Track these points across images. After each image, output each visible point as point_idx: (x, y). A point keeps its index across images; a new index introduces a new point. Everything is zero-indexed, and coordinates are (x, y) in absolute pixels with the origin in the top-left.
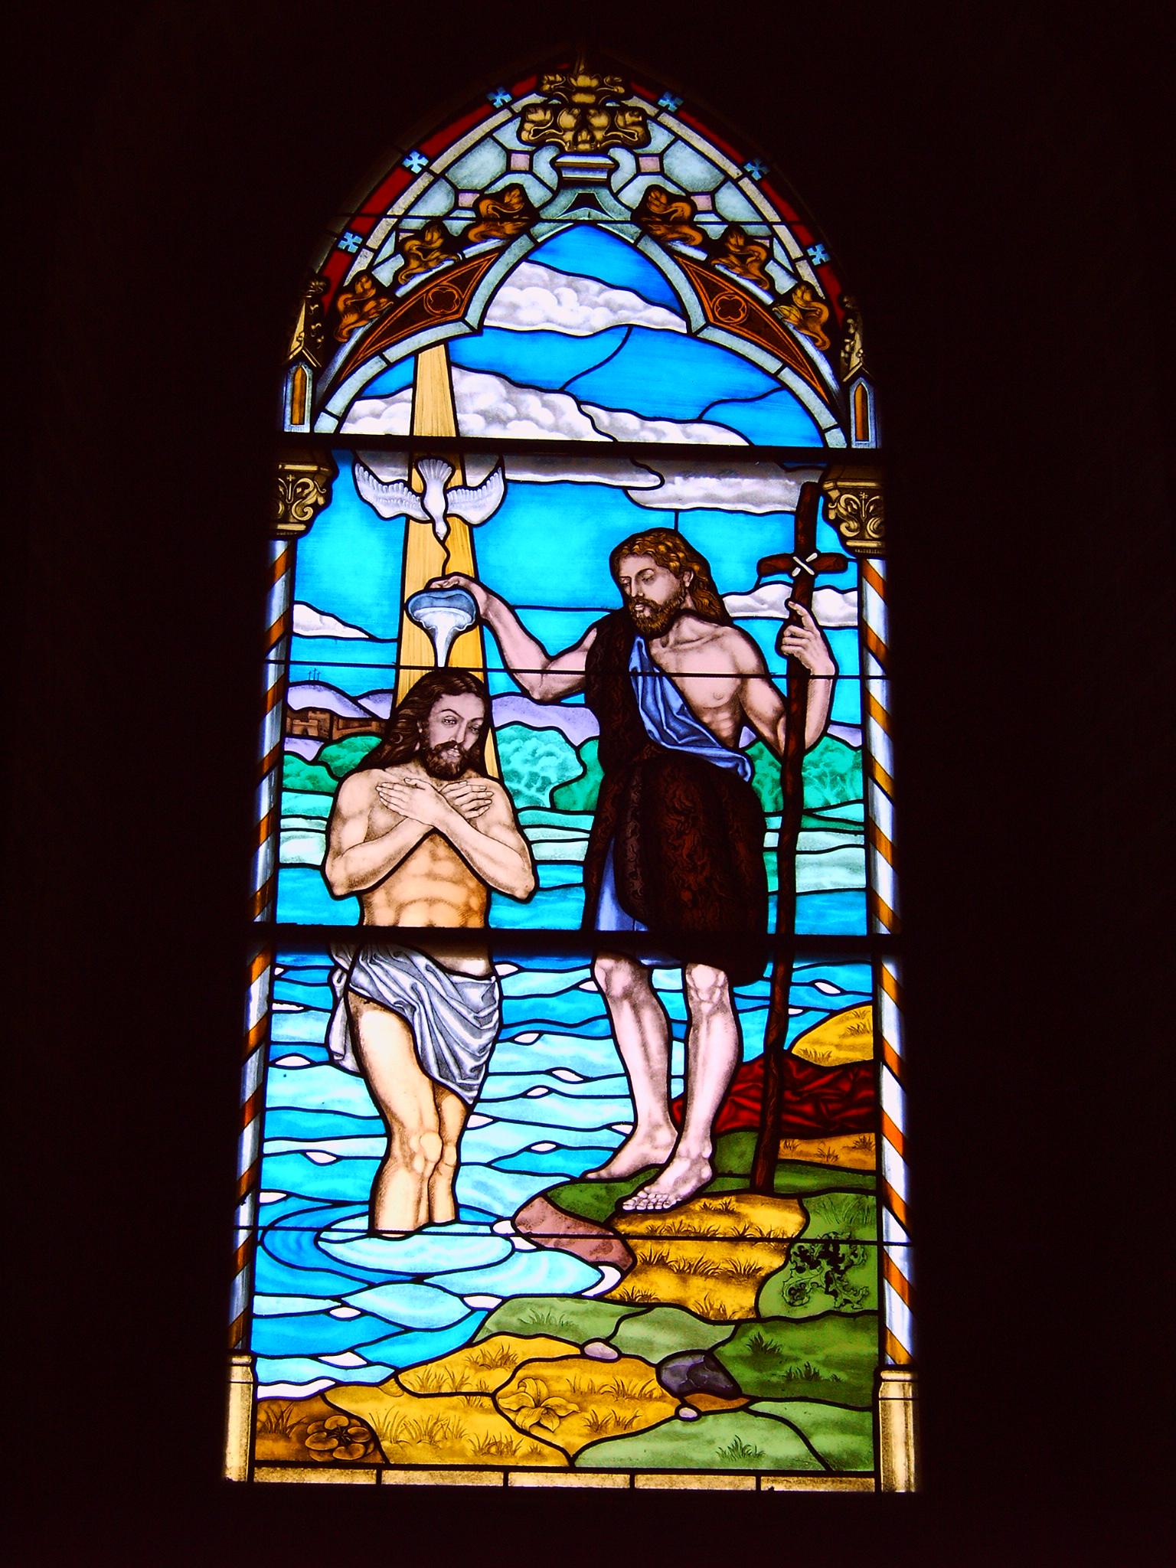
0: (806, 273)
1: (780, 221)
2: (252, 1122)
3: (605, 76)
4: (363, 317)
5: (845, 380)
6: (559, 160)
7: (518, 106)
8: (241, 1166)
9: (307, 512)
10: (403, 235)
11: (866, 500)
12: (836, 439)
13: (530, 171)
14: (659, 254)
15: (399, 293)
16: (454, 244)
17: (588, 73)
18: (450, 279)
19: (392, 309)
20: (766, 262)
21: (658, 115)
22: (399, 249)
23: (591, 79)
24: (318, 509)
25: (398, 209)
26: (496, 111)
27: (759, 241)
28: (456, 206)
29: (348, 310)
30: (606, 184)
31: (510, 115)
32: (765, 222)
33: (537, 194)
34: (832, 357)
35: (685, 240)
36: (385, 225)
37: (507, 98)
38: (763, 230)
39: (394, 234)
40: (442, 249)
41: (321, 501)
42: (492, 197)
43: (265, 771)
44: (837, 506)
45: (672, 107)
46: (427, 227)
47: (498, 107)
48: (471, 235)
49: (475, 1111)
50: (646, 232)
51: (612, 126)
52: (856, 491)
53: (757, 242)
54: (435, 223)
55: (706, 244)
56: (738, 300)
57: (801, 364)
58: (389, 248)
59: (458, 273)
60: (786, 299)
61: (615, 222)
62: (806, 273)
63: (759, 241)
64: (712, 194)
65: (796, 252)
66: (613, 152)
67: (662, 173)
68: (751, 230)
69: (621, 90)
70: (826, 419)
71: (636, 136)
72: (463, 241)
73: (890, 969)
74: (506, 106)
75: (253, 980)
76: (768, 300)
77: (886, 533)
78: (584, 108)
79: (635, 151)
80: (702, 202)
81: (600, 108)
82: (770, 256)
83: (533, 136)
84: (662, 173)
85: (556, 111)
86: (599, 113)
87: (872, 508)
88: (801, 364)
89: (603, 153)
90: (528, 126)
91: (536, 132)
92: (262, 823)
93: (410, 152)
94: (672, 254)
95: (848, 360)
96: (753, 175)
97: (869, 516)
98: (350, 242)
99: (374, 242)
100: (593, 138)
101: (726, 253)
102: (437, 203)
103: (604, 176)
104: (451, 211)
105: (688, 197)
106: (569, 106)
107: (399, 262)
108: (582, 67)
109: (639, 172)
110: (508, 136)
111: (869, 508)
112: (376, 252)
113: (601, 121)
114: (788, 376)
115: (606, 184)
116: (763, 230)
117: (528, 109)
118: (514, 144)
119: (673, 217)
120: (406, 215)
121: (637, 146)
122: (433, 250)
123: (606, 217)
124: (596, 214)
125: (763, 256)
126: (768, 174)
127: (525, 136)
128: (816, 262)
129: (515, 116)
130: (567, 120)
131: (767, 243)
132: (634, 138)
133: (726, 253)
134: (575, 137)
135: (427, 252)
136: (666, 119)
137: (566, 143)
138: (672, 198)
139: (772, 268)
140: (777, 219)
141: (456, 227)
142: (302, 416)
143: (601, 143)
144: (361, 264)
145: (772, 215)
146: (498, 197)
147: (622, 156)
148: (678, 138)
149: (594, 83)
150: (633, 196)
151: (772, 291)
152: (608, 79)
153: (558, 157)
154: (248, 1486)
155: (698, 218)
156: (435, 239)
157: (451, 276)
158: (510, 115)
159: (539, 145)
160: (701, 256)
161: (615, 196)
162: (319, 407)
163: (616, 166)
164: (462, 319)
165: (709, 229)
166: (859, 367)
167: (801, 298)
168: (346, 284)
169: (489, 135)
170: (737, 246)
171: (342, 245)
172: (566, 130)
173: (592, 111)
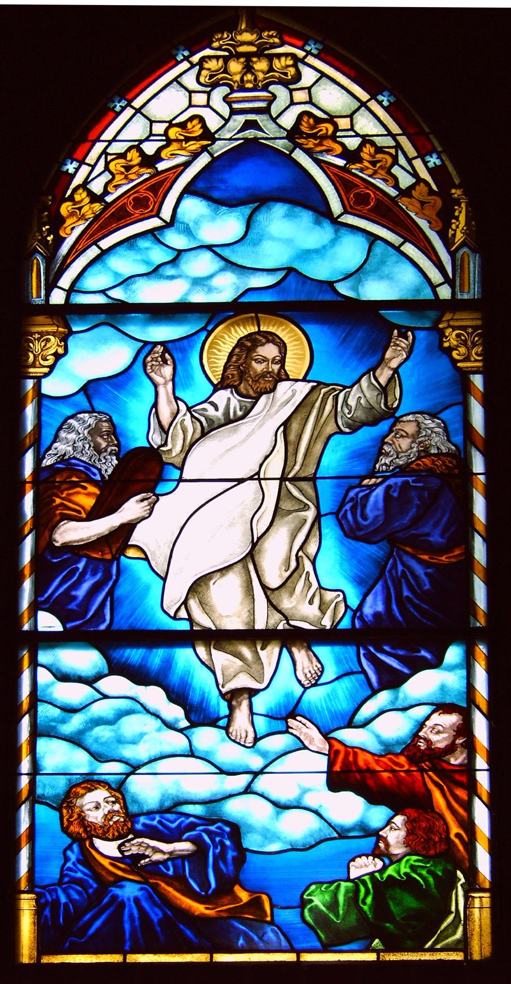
0: (424, 174)
2: (28, 845)
5: (452, 250)
6: (230, 96)
7: (195, 59)
8: (21, 737)
9: (48, 360)
10: (109, 158)
12: (445, 293)
13: (208, 105)
15: (109, 199)
18: (145, 187)
19: (103, 211)
20: (392, 166)
21: (305, 57)
22: (107, 168)
24: (58, 357)
25: (108, 135)
26: (118, 114)
27: (387, 150)
28: (151, 134)
31: (188, 65)
32: (390, 133)
33: (213, 123)
36: (99, 147)
37: (186, 53)
38: (389, 142)
39: (104, 156)
40: (141, 165)
41: (61, 351)
42: (177, 125)
43: (23, 799)
45: (315, 52)
48: (163, 155)
51: (271, 69)
52: (464, 328)
54: (137, 146)
55: (346, 154)
56: (369, 193)
57: (416, 237)
58: (101, 166)
59: (153, 181)
60: (407, 193)
61: (271, 139)
62: (424, 174)
63: (387, 150)
64: (351, 116)
67: (310, 102)
68: (380, 141)
69: (277, 40)
70: (435, 276)
71: (289, 75)
72: (157, 157)
74: (186, 59)
76: (393, 192)
78: (248, 56)
80: (343, 123)
81: (260, 54)
82: (395, 162)
83: (209, 79)
84: (310, 102)
85: (226, 60)
86: (260, 59)
88: (416, 237)
89: (265, 88)
90: (204, 73)
91: (211, 77)
92: (22, 837)
93: (113, 96)
95: (454, 235)
96: (384, 103)
97: (474, 345)
101: (361, 160)
103: (263, 105)
105: (331, 119)
106: (238, 55)
107: (106, 177)
109: (292, 103)
110: (189, 80)
111: (474, 339)
112: (93, 167)
114: (409, 249)
115: (266, 111)
117: (203, 60)
118: (193, 85)
120: (114, 140)
122: (133, 166)
125: (390, 160)
126: (394, 102)
127: (202, 80)
129: (193, 66)
131: (393, 151)
132: (288, 76)
135: (128, 168)
136: (310, 60)
137: (234, 83)
138: (318, 121)
139: (396, 170)
141: (150, 148)
142: (323, 404)
143: (262, 82)
144: (78, 180)
145: (395, 129)
146: (183, 125)
147: (280, 92)
148: (323, 75)
149: (254, 37)
150: (288, 121)
151: (396, 186)
152: (266, 34)
154: (37, 967)
158: (188, 65)
159: (214, 85)
160: (341, 162)
161: (274, 120)
162: (51, 285)
163: (274, 97)
165: (346, 141)
168: (67, 196)
169: (175, 80)
172: (236, 74)
173: (255, 59)
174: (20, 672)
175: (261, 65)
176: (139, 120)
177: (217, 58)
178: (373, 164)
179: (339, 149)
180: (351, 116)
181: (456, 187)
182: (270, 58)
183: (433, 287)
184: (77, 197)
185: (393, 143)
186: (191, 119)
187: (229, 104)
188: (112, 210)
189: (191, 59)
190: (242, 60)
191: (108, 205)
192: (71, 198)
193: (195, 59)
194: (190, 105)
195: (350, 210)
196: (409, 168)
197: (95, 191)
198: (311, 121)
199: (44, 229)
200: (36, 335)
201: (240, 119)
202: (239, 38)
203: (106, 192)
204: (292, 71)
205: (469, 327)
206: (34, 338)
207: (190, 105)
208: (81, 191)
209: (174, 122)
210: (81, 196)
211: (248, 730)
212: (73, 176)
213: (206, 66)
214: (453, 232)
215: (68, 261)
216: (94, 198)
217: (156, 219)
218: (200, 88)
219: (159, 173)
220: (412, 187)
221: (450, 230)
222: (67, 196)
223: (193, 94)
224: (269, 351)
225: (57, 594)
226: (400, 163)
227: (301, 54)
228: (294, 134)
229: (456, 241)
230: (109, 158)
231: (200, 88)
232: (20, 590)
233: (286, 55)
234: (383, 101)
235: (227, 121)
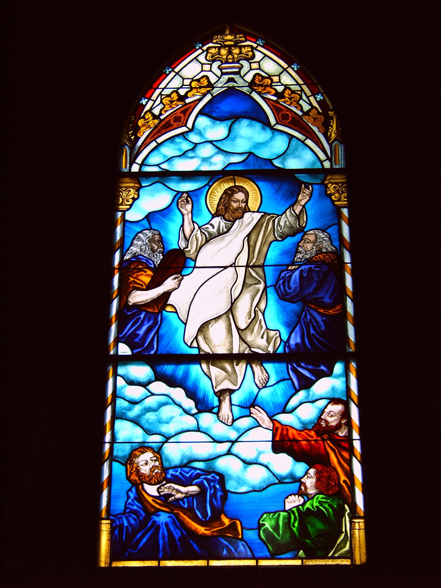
0: (315, 104)
1: (301, 86)
3: (237, 34)
4: (149, 127)
5: (330, 142)
6: (221, 66)
7: (205, 48)
10: (163, 97)
11: (342, 186)
12: (327, 165)
13: (210, 71)
14: (258, 99)
15: (162, 117)
17: (231, 34)
19: (159, 123)
20: (299, 100)
21: (257, 47)
22: (161, 102)
23: (232, 36)
25: (162, 85)
26: (197, 50)
27: (297, 92)
29: (144, 125)
30: (238, 73)
31: (202, 51)
32: (298, 84)
33: (213, 79)
35: (268, 93)
36: (158, 91)
37: (200, 45)
38: (297, 88)
39: (160, 96)
40: (178, 100)
42: (196, 80)
43: (106, 458)
44: (330, 190)
45: (261, 44)
46: (172, 92)
47: (197, 49)
48: (189, 95)
49: (194, 416)
51: (241, 53)
53: (296, 93)
55: (277, 94)
60: (307, 113)
62: (315, 104)
63: (297, 92)
64: (279, 76)
66: (241, 62)
67: (260, 69)
69: (243, 39)
70: (322, 156)
71: (249, 55)
72: (186, 96)
73: (353, 365)
74: (200, 48)
75: (115, 315)
76: (300, 113)
77: (349, 198)
78: (230, 46)
79: (250, 61)
80: (275, 79)
81: (235, 46)
82: (301, 98)
83: (211, 58)
84: (260, 69)
85: (219, 48)
86: (235, 48)
87: (344, 189)
89: (238, 62)
90: (209, 55)
91: (212, 57)
93: (165, 66)
94: (264, 99)
95: (331, 135)
96: (295, 69)
97: (343, 192)
98: (144, 102)
100: (233, 58)
101: (284, 97)
102: (176, 83)
104: (182, 86)
105: (270, 77)
106: (225, 46)
107: (161, 106)
108: (228, 32)
109: (251, 69)
110: (202, 58)
112: (155, 101)
113: (236, 51)
114: (309, 142)
115: (238, 73)
116: (297, 88)
117: (208, 48)
118: (203, 61)
119: (264, 84)
121: (250, 59)
122: (174, 101)
123: (238, 85)
124: (235, 85)
125: (298, 97)
127: (208, 58)
128: (318, 99)
130: (224, 52)
131: (300, 93)
132: (249, 56)
133: (284, 97)
134: (227, 57)
135: (172, 102)
136: (259, 48)
137: (223, 60)
138: (263, 78)
139: (301, 102)
140: (302, 83)
141: (182, 92)
143: (236, 59)
144: (147, 108)
145: (300, 82)
146: (198, 80)
148: (265, 55)
150: (249, 78)
151: (302, 110)
156: (175, 96)
157: (179, 111)
158: (202, 51)
159: (214, 61)
160: (274, 98)
161: (242, 78)
162: (132, 162)
164: (185, 126)
165: (276, 87)
166: (335, 137)
167: (313, 113)
168: (141, 116)
169: (195, 58)
171: (141, 102)
173: (233, 48)
176: (178, 79)
179: (273, 92)
180: (279, 76)
181: (331, 111)
183: (321, 162)
185: (299, 89)
186: (203, 77)
187: (221, 70)
189: (202, 48)
190: (227, 48)
191: (162, 121)
192: (144, 117)
193: (205, 48)
194: (202, 71)
196: (308, 101)
198: (260, 78)
199: (130, 133)
200: (124, 188)
201: (226, 77)
202: (225, 38)
203: (161, 114)
204: (250, 54)
206: (123, 190)
207: (202, 71)
208: (148, 113)
209: (194, 79)
210: (149, 116)
213: (210, 51)
214: (330, 133)
215: (141, 149)
216: (155, 117)
217: (185, 127)
220: (309, 111)
221: (329, 132)
228: (252, 84)
229: (332, 138)
233: (248, 46)
234: (294, 68)
235: (220, 78)
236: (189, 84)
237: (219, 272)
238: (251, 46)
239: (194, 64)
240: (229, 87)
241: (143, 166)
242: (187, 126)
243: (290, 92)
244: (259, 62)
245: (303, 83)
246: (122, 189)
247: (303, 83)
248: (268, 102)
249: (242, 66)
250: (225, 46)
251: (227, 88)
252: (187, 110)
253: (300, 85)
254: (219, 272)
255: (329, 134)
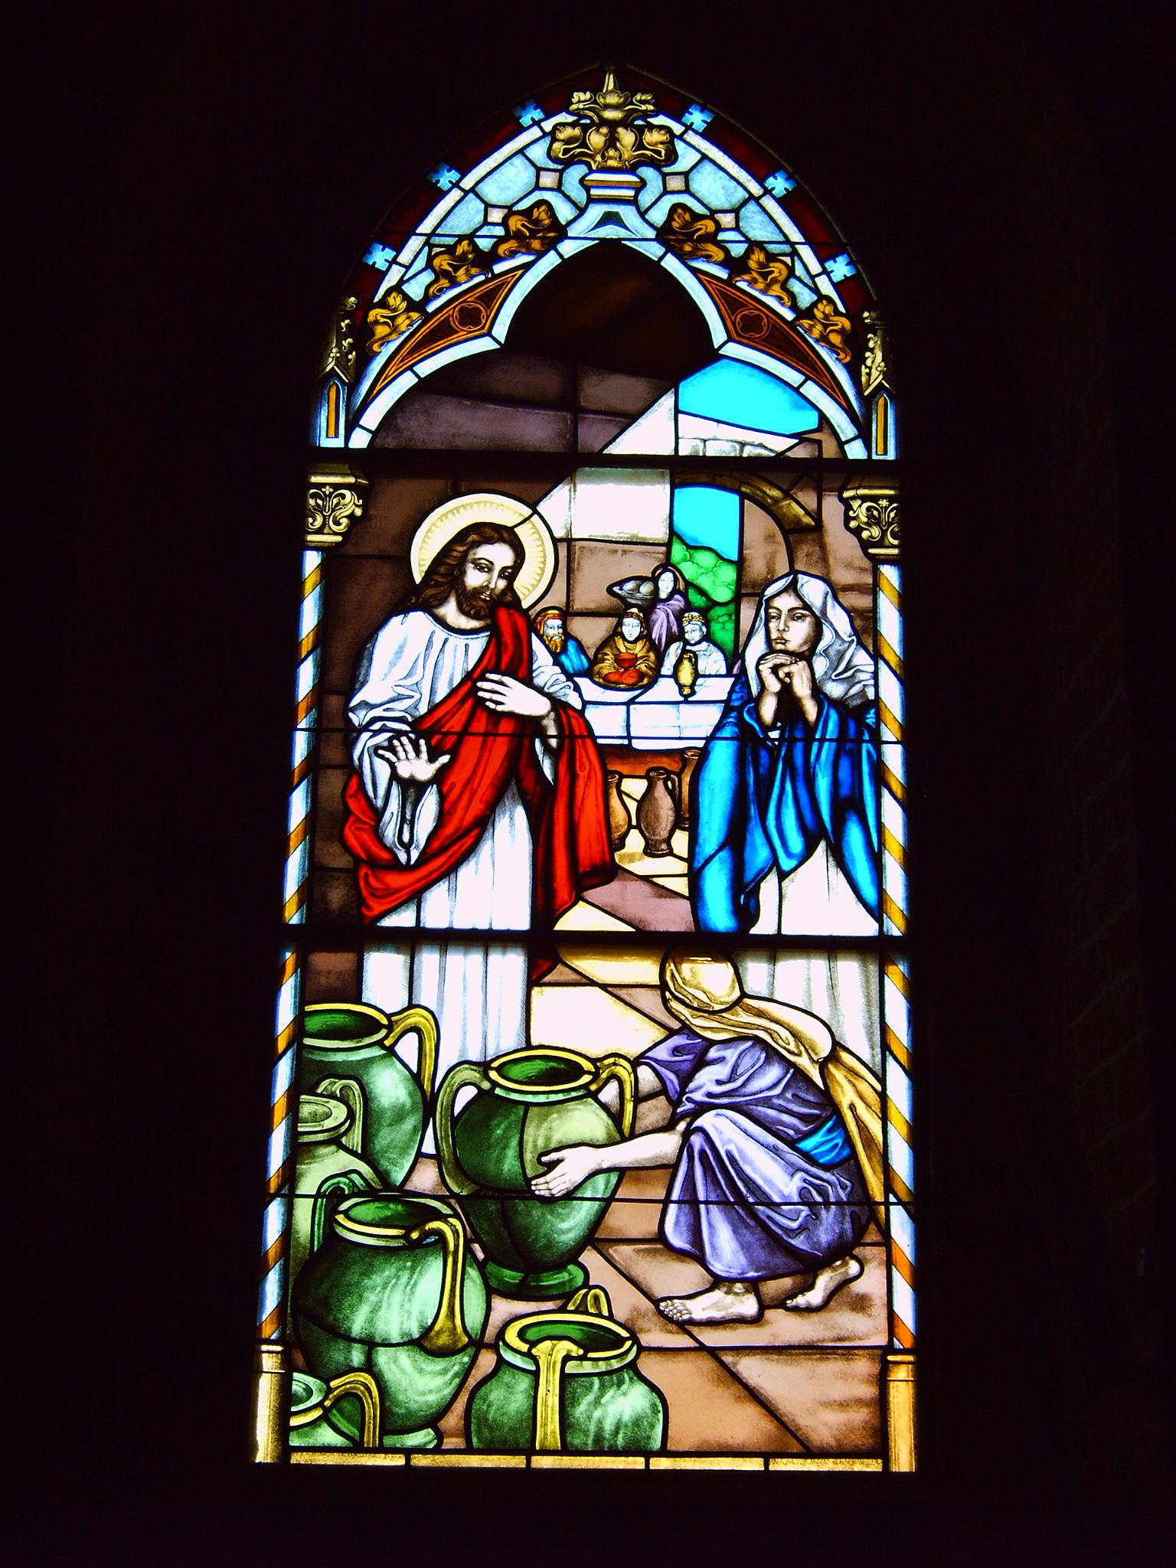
7: (548, 126)
10: (436, 250)
16: (485, 260)
22: (429, 265)
25: (426, 227)
28: (486, 223)
31: (540, 134)
32: (787, 241)
33: (564, 212)
34: (854, 370)
36: (414, 243)
42: (519, 213)
50: (670, 249)
58: (421, 262)
60: (808, 313)
65: (815, 267)
67: (687, 190)
68: (774, 248)
76: (789, 316)
78: (613, 125)
80: (727, 220)
81: (626, 123)
83: (563, 155)
84: (687, 190)
85: (585, 129)
89: (632, 170)
99: (405, 257)
101: (748, 270)
102: (466, 219)
105: (713, 213)
107: (427, 277)
109: (666, 192)
110: (538, 153)
112: (408, 268)
114: (811, 390)
115: (634, 202)
116: (786, 248)
117: (555, 127)
125: (785, 272)
128: (837, 277)
130: (596, 140)
131: (788, 260)
133: (748, 270)
136: (691, 137)
145: (795, 236)
147: (647, 173)
148: (704, 157)
150: (658, 216)
151: (794, 307)
153: (586, 175)
155: (722, 236)
158: (540, 134)
159: (568, 163)
160: (723, 274)
161: (642, 214)
162: (353, 424)
168: (376, 300)
169: (521, 152)
170: (759, 263)
174: (268, 1130)
175: (627, 137)
176: (474, 206)
177: (573, 125)
178: (765, 276)
179: (720, 255)
180: (736, 211)
182: (639, 131)
184: (391, 301)
186: (539, 204)
187: (587, 189)
188: (432, 323)
189: (543, 124)
190: (604, 130)
191: (428, 317)
192: (383, 304)
193: (548, 126)
194: (537, 187)
195: (737, 338)
196: (810, 283)
197: (412, 296)
198: (687, 217)
199: (343, 324)
200: (327, 487)
201: (596, 212)
202: (601, 100)
203: (427, 298)
205: (883, 497)
206: (324, 493)
207: (537, 187)
208: (394, 294)
209: (515, 209)
210: (395, 300)
211: (474, 873)
212: (382, 275)
213: (561, 136)
214: (867, 370)
215: (375, 392)
216: (412, 306)
217: (487, 339)
218: (552, 165)
219: (495, 277)
220: (814, 305)
221: (863, 367)
222: (376, 300)
223: (542, 173)
224: (500, 555)
225: (363, 1199)
226: (797, 273)
227: (678, 129)
228: (664, 234)
230: (436, 250)
231: (552, 165)
232: (321, 617)
233: (661, 127)
236: (500, 221)
237: (493, 854)
238: (669, 130)
239: (519, 161)
240: (603, 240)
241: (402, 1455)
242: (526, 126)
243: (762, 257)
244: (686, 175)
245: (803, 241)
246: (323, 490)
247: (803, 241)
248: (708, 285)
249: (643, 183)
250: (604, 122)
251: (598, 241)
252: (498, 288)
253: (792, 244)
254: (493, 854)
255: (864, 370)
